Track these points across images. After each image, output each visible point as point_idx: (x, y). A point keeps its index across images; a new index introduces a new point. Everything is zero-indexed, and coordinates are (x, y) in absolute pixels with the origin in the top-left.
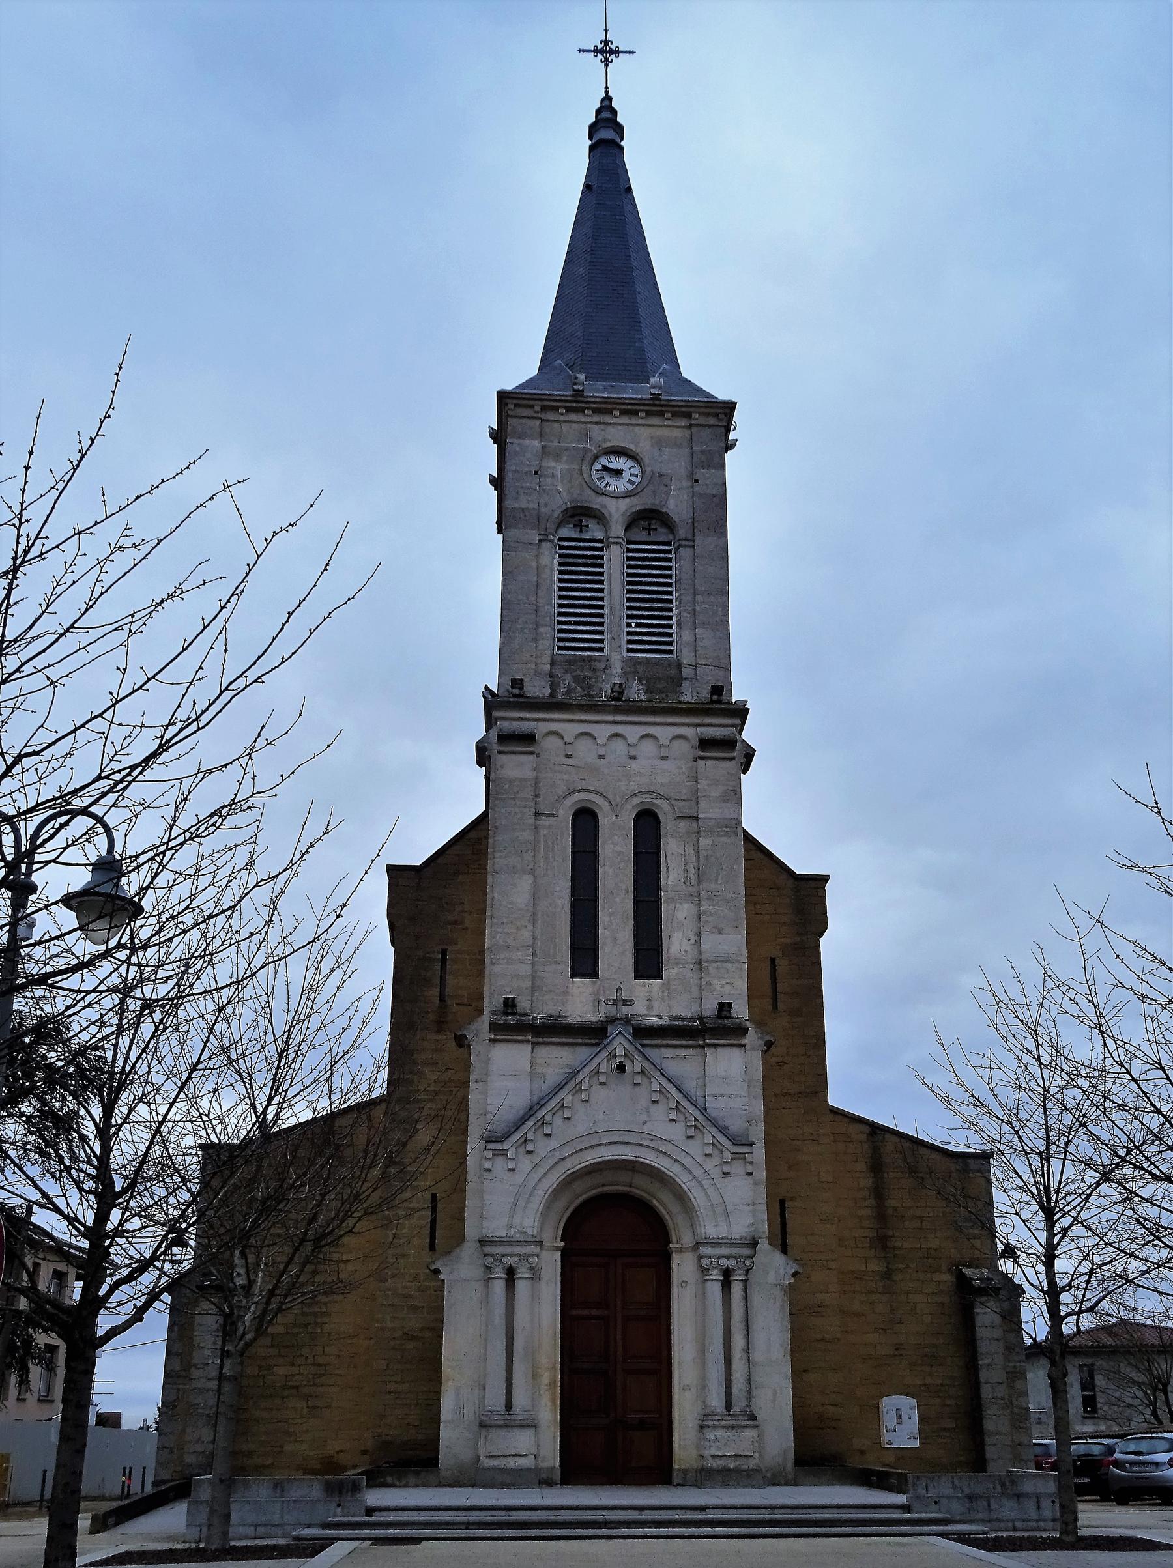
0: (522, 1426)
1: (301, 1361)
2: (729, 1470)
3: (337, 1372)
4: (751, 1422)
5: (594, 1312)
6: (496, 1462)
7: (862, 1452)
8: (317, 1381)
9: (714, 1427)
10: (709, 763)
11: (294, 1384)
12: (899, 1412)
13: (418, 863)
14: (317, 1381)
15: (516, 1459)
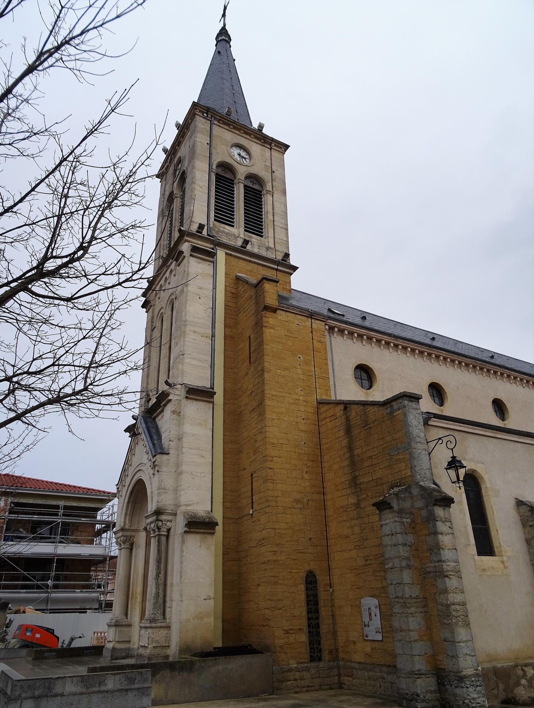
7: (354, 643)
12: (370, 611)
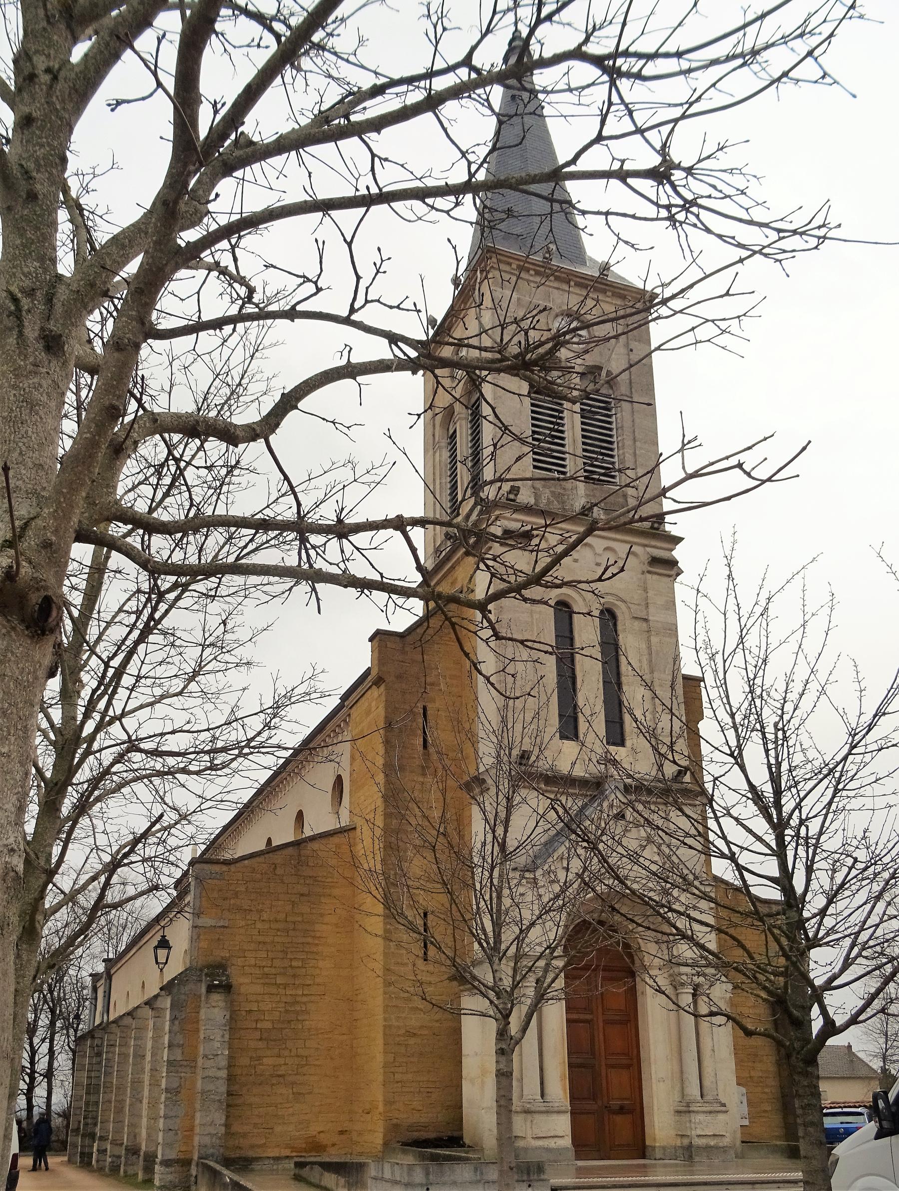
0: (559, 1112)
1: (286, 1053)
2: (711, 1147)
3: (317, 1063)
4: (723, 1109)
5: (582, 1017)
6: (540, 1143)
8: (300, 1070)
9: (697, 1112)
10: (655, 577)
11: (280, 1073)
13: (401, 631)
14: (300, 1070)
15: (556, 1140)
